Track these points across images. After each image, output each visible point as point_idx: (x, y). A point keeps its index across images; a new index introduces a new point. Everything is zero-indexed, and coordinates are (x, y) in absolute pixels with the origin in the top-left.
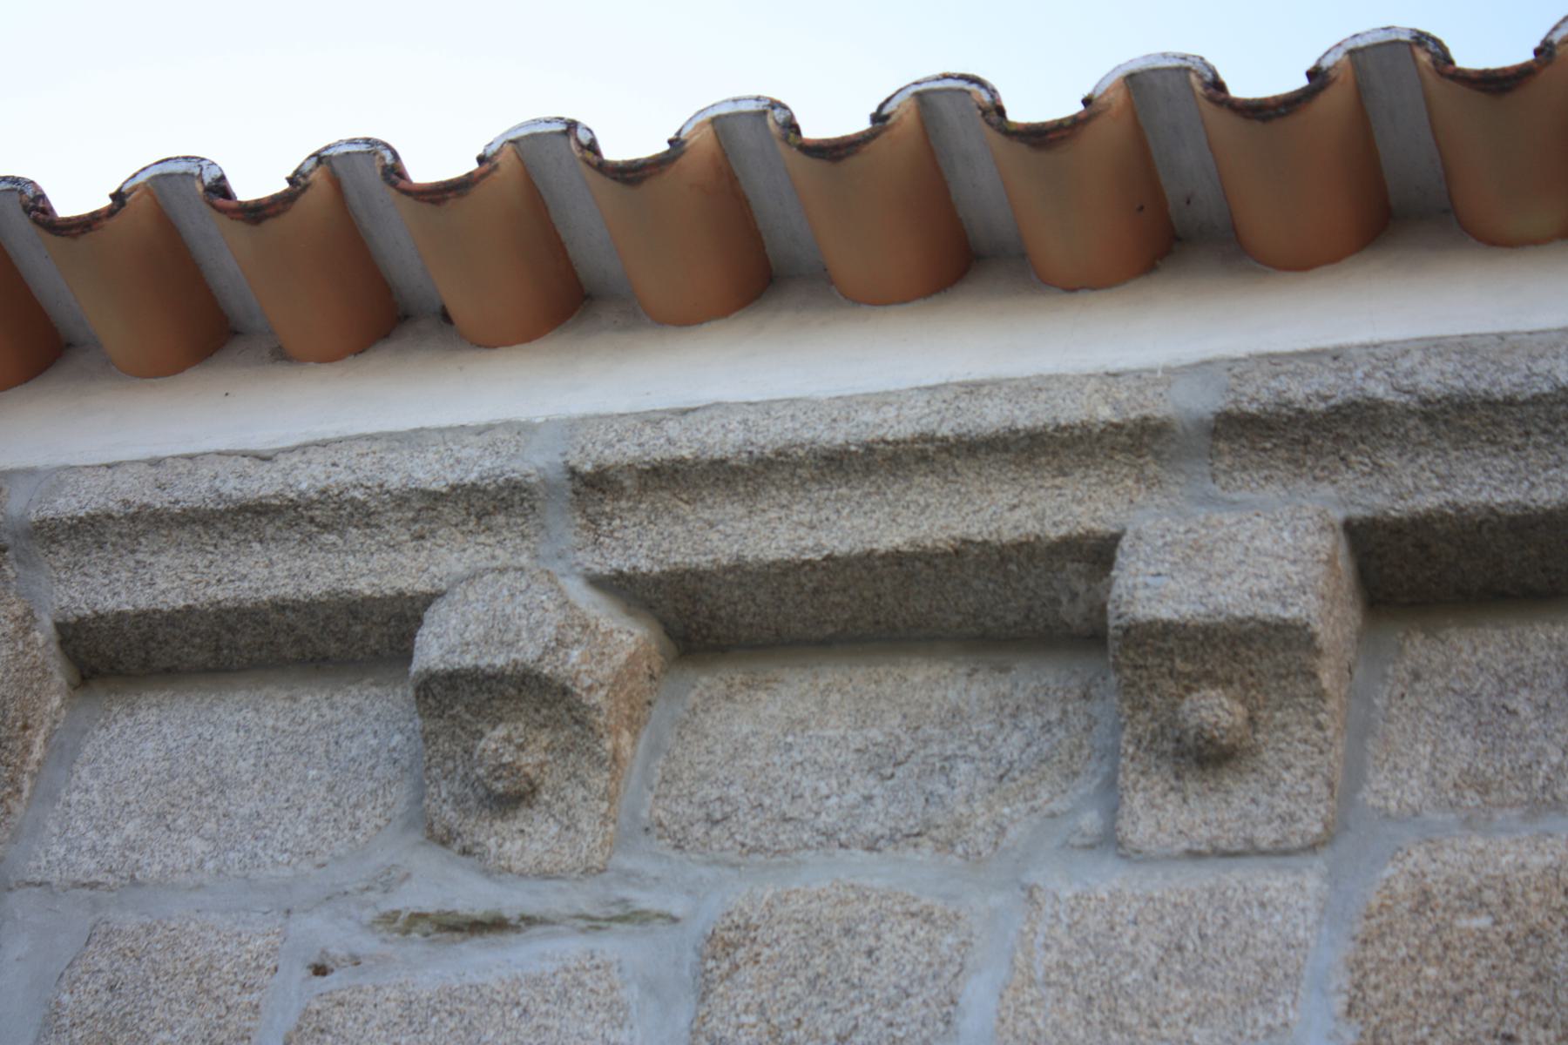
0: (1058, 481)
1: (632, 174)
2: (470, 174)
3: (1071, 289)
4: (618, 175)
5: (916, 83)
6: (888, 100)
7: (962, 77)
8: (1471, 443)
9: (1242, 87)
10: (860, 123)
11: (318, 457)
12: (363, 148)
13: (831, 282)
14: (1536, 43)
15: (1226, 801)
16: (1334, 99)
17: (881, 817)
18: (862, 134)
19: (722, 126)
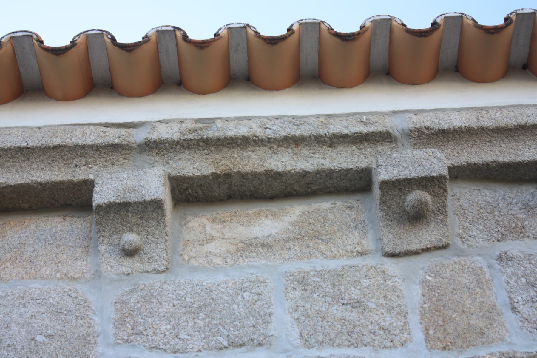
0: (329, 149)
1: (202, 45)
2: (66, 46)
3: (60, 100)
4: (197, 45)
5: (13, 33)
6: (3, 37)
7: (10, 33)
8: (429, 146)
9: (193, 36)
10: (210, 36)
11: (79, 130)
12: (100, 32)
13: (45, 92)
14: (143, 35)
15: (188, 228)
16: (149, 47)
17: (485, 230)
18: (212, 39)
19: (160, 33)
